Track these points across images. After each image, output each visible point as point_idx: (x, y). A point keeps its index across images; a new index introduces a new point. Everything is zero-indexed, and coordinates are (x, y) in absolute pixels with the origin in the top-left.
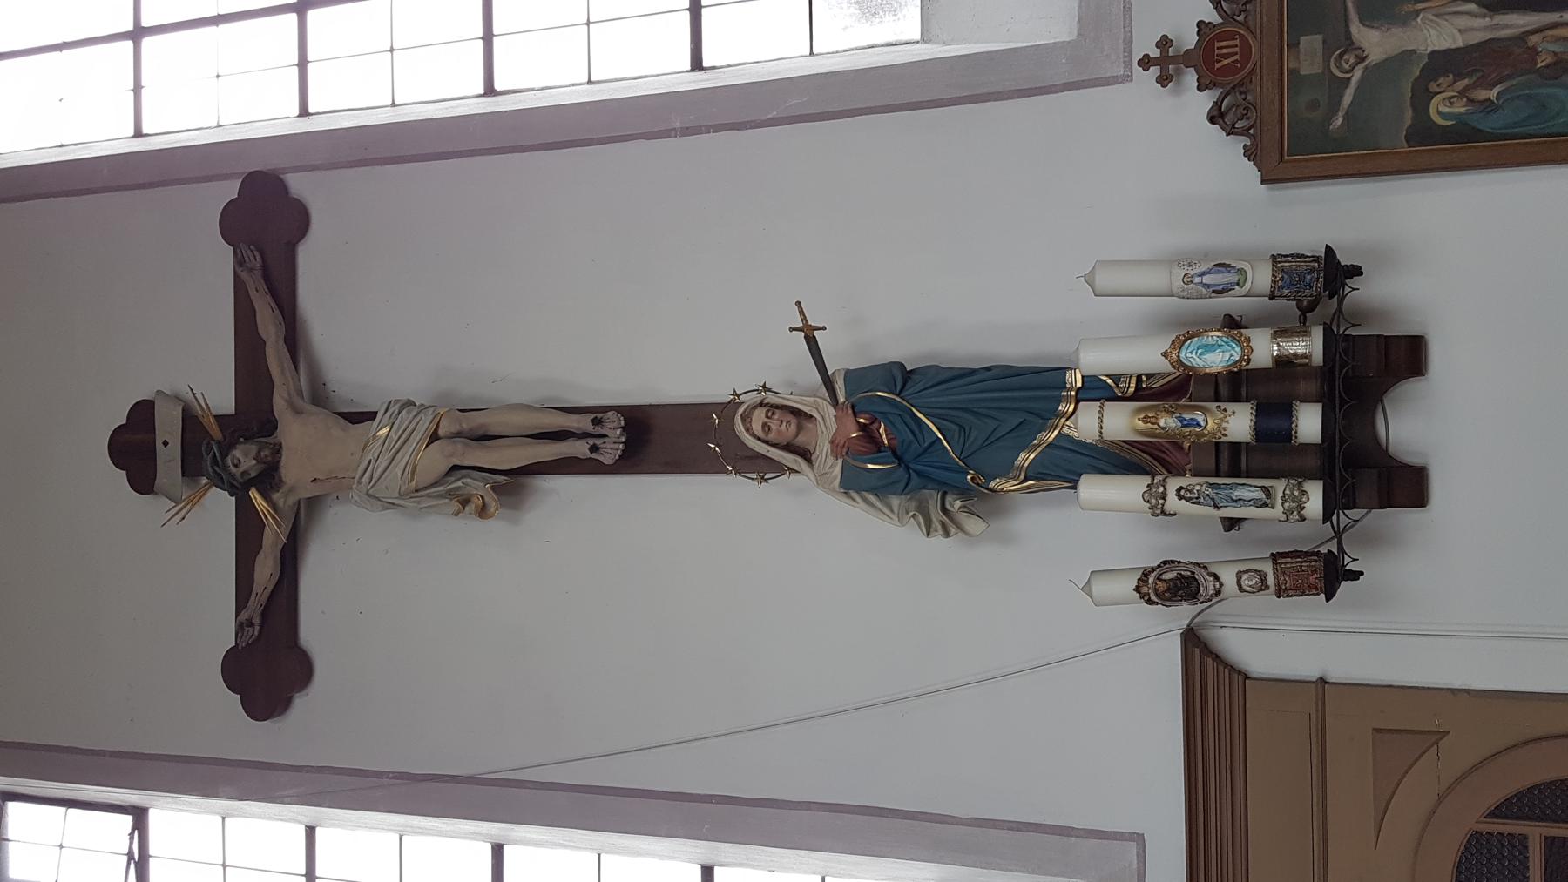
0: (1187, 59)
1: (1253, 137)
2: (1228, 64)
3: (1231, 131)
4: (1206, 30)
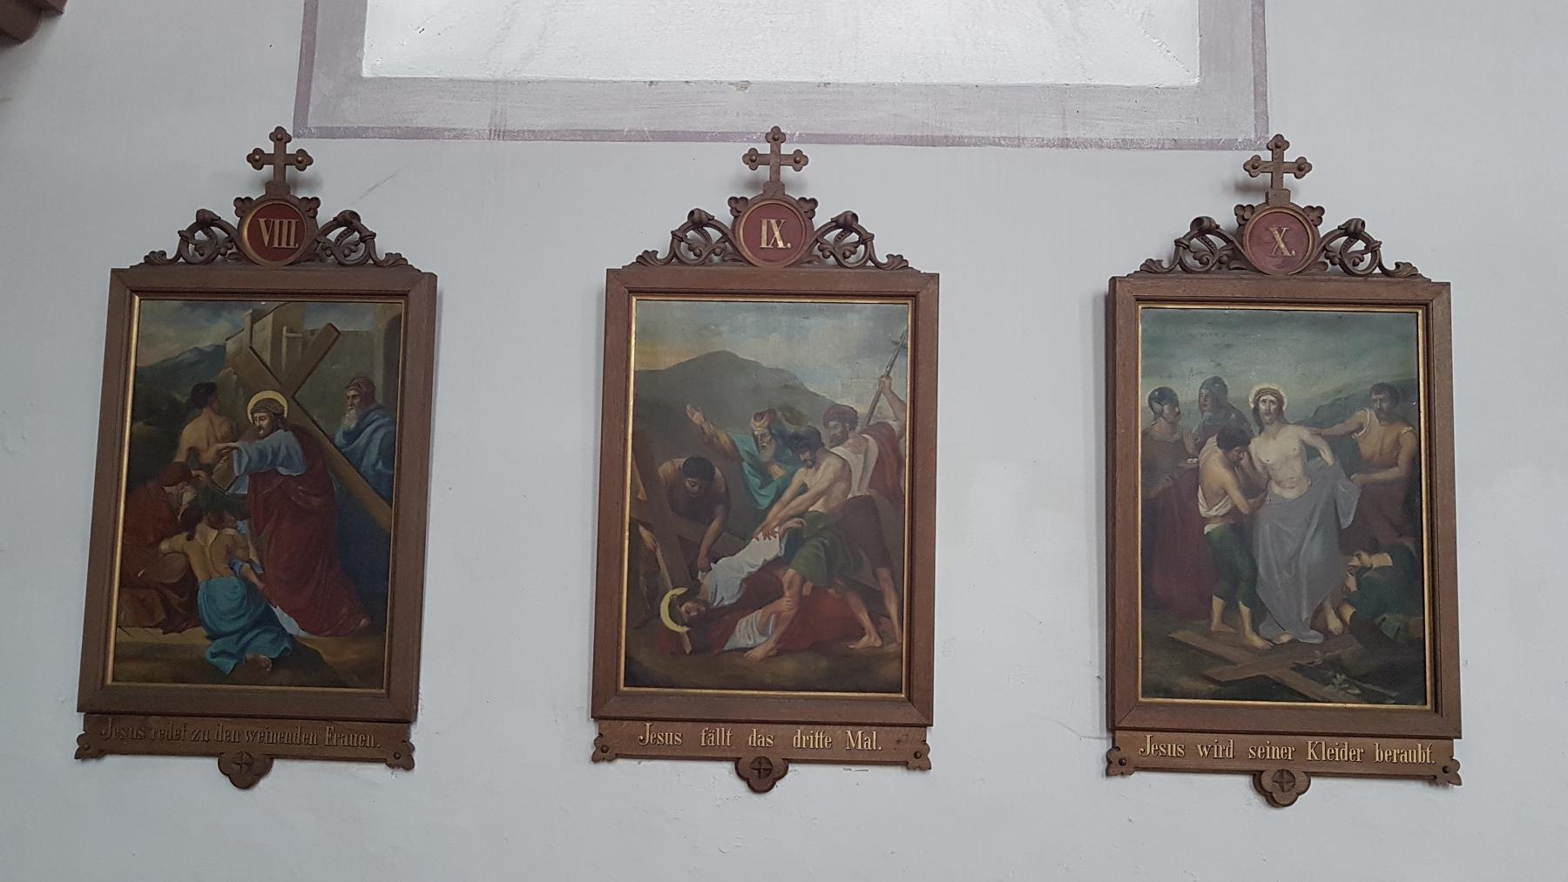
0: (1276, 196)
1: (668, 261)
2: (1276, 242)
3: (186, 237)
4: (807, 207)
